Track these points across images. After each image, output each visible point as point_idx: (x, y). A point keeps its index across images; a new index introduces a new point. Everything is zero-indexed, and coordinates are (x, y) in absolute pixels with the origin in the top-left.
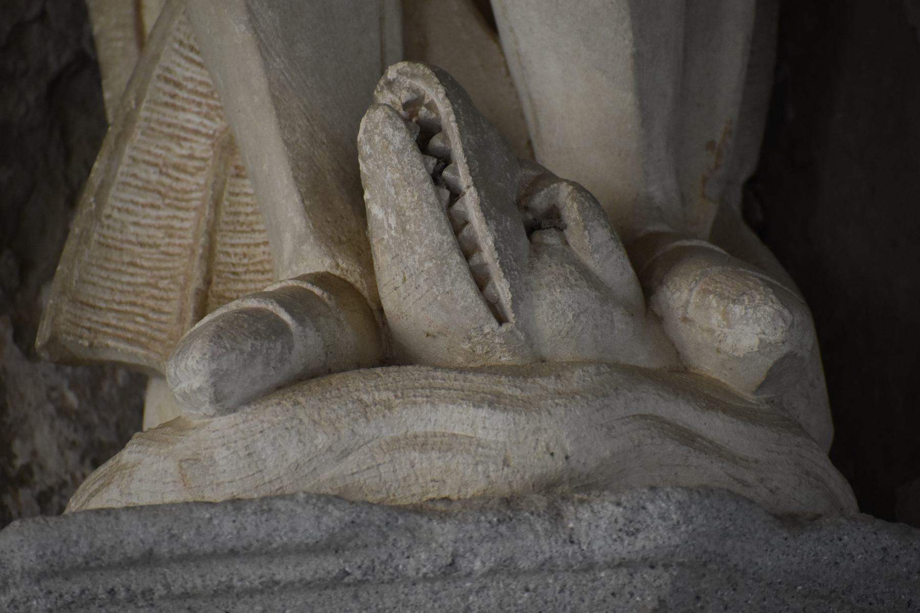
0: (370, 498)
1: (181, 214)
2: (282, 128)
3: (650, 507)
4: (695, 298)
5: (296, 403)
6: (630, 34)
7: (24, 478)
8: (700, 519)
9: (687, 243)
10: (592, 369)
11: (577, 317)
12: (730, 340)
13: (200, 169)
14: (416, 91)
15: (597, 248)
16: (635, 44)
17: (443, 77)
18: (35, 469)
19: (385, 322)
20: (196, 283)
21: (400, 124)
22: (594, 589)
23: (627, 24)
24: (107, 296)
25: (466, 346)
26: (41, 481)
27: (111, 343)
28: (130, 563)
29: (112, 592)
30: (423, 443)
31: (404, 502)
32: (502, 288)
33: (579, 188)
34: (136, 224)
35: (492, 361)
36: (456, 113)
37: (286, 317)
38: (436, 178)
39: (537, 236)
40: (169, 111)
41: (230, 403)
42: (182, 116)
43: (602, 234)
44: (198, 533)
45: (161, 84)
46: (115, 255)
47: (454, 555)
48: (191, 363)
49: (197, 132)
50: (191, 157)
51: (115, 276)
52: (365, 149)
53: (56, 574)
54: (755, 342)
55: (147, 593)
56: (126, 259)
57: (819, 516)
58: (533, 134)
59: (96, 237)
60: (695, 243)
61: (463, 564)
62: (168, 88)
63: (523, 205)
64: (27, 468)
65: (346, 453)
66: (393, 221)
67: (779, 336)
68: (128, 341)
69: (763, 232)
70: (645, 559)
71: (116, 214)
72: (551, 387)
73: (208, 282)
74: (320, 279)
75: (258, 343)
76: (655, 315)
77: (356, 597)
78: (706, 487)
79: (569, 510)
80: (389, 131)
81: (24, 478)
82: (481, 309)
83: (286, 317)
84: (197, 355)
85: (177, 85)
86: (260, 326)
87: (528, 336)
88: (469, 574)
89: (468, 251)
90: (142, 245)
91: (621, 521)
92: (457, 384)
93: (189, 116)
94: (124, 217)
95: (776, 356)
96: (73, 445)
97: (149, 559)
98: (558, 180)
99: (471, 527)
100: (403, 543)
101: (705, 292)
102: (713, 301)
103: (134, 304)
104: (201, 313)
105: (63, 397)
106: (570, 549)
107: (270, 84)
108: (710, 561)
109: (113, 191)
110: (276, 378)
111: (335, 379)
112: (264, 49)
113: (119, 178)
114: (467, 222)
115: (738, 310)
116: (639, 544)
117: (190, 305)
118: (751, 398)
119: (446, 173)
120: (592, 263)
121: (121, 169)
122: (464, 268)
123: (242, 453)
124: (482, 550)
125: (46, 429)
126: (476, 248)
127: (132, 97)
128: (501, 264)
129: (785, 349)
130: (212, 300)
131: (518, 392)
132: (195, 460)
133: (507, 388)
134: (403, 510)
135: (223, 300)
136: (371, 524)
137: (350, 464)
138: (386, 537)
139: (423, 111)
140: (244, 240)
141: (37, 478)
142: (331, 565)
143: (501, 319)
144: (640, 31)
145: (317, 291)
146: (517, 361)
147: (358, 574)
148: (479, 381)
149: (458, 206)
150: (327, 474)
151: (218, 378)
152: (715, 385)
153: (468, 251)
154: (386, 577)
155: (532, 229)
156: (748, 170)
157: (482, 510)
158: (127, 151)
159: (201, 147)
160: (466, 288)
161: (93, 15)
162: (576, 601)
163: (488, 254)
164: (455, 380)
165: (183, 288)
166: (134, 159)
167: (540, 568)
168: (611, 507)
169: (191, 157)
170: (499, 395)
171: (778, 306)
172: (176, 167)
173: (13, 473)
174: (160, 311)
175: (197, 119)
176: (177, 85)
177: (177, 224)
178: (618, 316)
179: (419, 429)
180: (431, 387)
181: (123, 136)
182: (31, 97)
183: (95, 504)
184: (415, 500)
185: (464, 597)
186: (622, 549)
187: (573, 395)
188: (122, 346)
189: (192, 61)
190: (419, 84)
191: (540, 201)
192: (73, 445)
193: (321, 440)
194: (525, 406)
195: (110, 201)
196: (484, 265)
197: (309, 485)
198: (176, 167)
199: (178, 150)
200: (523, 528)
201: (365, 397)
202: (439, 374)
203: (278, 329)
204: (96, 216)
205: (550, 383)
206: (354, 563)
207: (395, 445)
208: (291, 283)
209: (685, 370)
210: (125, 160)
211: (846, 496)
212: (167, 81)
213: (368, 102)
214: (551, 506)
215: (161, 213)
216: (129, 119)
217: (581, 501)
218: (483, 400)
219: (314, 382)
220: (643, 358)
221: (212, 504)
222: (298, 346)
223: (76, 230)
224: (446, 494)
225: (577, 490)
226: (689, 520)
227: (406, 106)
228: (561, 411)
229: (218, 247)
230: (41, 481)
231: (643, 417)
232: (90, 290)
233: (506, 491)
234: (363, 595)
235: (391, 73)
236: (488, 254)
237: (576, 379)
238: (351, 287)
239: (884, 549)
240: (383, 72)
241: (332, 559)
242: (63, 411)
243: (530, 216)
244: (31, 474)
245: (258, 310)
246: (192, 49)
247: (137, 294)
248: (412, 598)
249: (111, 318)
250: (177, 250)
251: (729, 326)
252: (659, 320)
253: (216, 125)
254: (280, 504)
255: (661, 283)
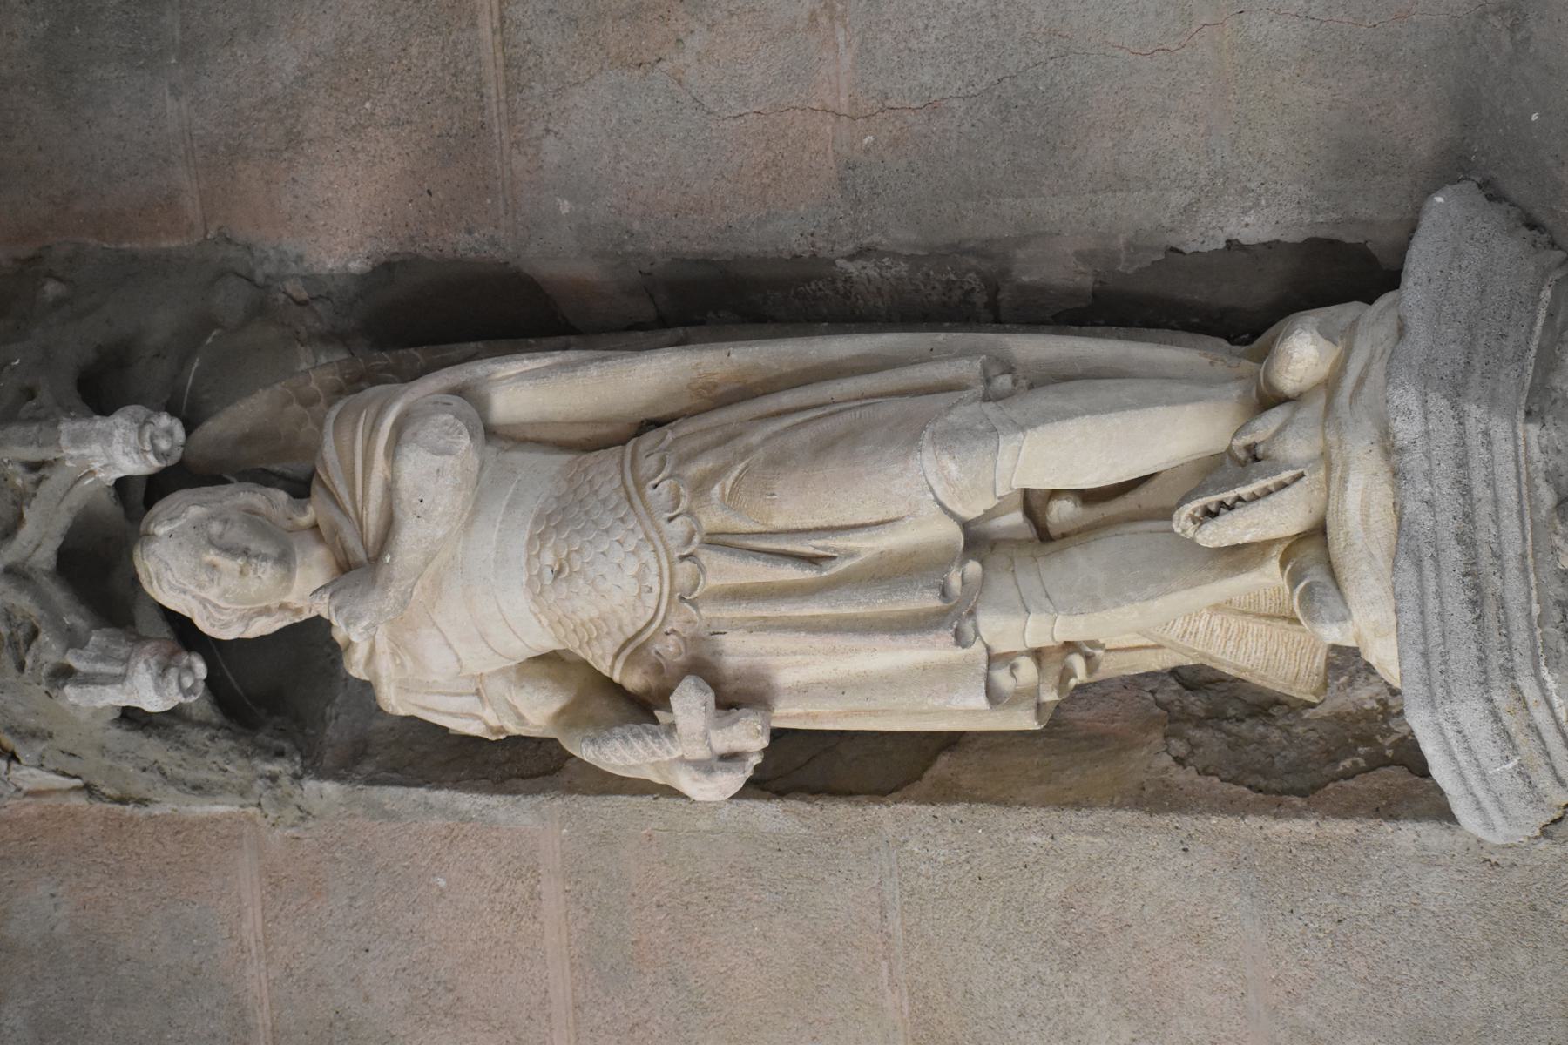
0: (1394, 542)
1: (1250, 631)
2: (1206, 583)
3: (1396, 403)
4: (1290, 377)
5: (1346, 580)
6: (1157, 408)
7: (1383, 703)
8: (1402, 378)
9: (1262, 380)
10: (1327, 430)
11: (1300, 437)
12: (1311, 359)
13: (1227, 621)
14: (1187, 518)
15: (1266, 427)
16: (1162, 405)
17: (1179, 505)
18: (1379, 697)
19: (1305, 532)
20: (1285, 623)
21: (1203, 526)
22: (1438, 430)
23: (1152, 409)
24: (1292, 667)
25: (1316, 493)
26: (1385, 694)
27: (1316, 665)
28: (1427, 664)
29: (1441, 672)
30: (1366, 516)
31: (1396, 526)
32: (1286, 475)
33: (1235, 435)
34: (1256, 652)
35: (1324, 480)
36: (1198, 498)
37: (1302, 585)
38: (1231, 508)
39: (1259, 457)
40: (1199, 635)
41: (1346, 613)
42: (1200, 630)
43: (1258, 424)
44: (1412, 630)
45: (1185, 640)
46: (1271, 663)
47: (1422, 501)
48: (1326, 633)
49: (1209, 623)
50: (1221, 625)
51: (1282, 663)
52: (1216, 544)
53: (1433, 700)
54: (1312, 347)
55: (1442, 655)
56: (1273, 657)
57: (1399, 317)
58: (1207, 455)
59: (1263, 672)
60: (1262, 374)
61: (1427, 497)
62: (1187, 636)
63: (1243, 464)
64: (1379, 701)
65: (1371, 555)
66: (1253, 530)
67: (1308, 335)
68: (1314, 657)
69: (1256, 335)
70: (1423, 406)
71: (1250, 662)
72: (1336, 451)
73: (1285, 618)
74: (1283, 564)
75: (1316, 599)
76: (1299, 396)
77: (1443, 551)
78: (1386, 375)
79: (1398, 444)
80: (1207, 532)
81: (1383, 703)
82: (1297, 485)
83: (1302, 585)
84: (1322, 630)
85: (1185, 632)
86: (1307, 598)
87: (1310, 462)
88: (1432, 494)
89: (1268, 492)
90: (1266, 650)
91: (1404, 418)
92: (1336, 499)
93: (1201, 626)
94: (1252, 658)
95: (1319, 337)
96: (1366, 678)
97: (1425, 654)
98: (1231, 445)
99: (1408, 493)
100: (1417, 527)
101: (1287, 371)
102: (1291, 368)
103: (1296, 654)
104: (1297, 621)
105: (1342, 684)
106: (1418, 444)
107: (1185, 589)
108: (1460, 732)
109: (1239, 663)
110: (1333, 589)
111: (1333, 560)
112: (1167, 592)
113: (1232, 660)
114: (1253, 493)
115: (1296, 356)
116: (1415, 408)
117: (1296, 627)
118: (1340, 348)
119: (1228, 503)
120: (1273, 429)
121: (1228, 658)
122: (1277, 494)
123: (1371, 607)
124: (1419, 487)
125: (1359, 692)
126: (1266, 488)
127: (1192, 654)
128: (1274, 475)
129: (1315, 332)
130: (1293, 616)
131: (1339, 468)
132: (1375, 630)
133: (1337, 474)
134: (1400, 528)
135: (1293, 611)
136: (1407, 544)
137: (1377, 553)
138: (1413, 536)
139: (1197, 515)
140: (1263, 600)
141: (1383, 697)
142: (1428, 564)
143: (1302, 475)
144: (1155, 403)
145: (1289, 567)
146: (1323, 467)
147: (1432, 550)
148: (1334, 487)
149: (1245, 497)
150: (1382, 565)
151: (1334, 619)
152: (1334, 366)
153: (1268, 492)
154: (1434, 536)
155: (1256, 459)
156: (1223, 343)
157: (1399, 487)
158: (1219, 656)
159: (1216, 620)
160: (1286, 494)
161: (1151, 669)
162: (1444, 440)
163: (1269, 482)
164: (1333, 500)
165: (1287, 629)
166: (1224, 652)
167: (1428, 458)
168: (1397, 423)
169: (1221, 625)
170: (1341, 478)
171: (1294, 336)
172: (1227, 632)
173: (1381, 708)
174: (1299, 643)
175: (1202, 622)
176: (1185, 632)
177: (1255, 632)
178: (1299, 415)
179: (1358, 518)
180: (1337, 512)
181: (1211, 659)
182: (1193, 699)
183: (1398, 677)
184: (1395, 520)
185: (1443, 496)
186: (1418, 417)
187: (1340, 441)
188: (1317, 660)
189: (1173, 624)
190: (1183, 517)
191: (1242, 455)
192: (1366, 678)
193: (1364, 567)
194: (1346, 464)
195: (1244, 665)
196: (1275, 484)
197: (1388, 574)
198: (1227, 632)
199: (1218, 632)
200: (1408, 467)
201: (1343, 545)
202: (1330, 508)
203: (1308, 588)
204: (1252, 672)
205: (1334, 452)
206: (1427, 552)
207: (1367, 530)
208: (1285, 579)
209: (1327, 380)
210: (1223, 657)
211: (1389, 297)
212: (1183, 637)
213: (1193, 540)
214: (1397, 452)
215: (1250, 640)
216: (1203, 655)
217: (1394, 437)
218: (1344, 486)
219: (1335, 571)
220: (1321, 402)
221: (1398, 623)
222: (1318, 578)
223: (1259, 682)
224: (1391, 505)
225: (1388, 438)
226: (1403, 384)
227: (1194, 523)
228: (1348, 446)
229: (1267, 612)
230: (1385, 694)
231: (1351, 404)
232: (1289, 676)
233: (1389, 474)
234: (1443, 547)
235: (1178, 530)
236: (1269, 482)
237: (1332, 438)
238: (1286, 550)
239: (1415, 284)
240: (1177, 534)
241: (1424, 563)
242: (1350, 683)
243: (1250, 460)
244: (1381, 699)
245: (1299, 599)
246: (1167, 624)
247: (1291, 652)
248: (1444, 522)
249: (1303, 665)
250: (1269, 633)
251: (1304, 360)
252: (1301, 394)
253: (1206, 614)
254: (1398, 589)
255: (1282, 393)
